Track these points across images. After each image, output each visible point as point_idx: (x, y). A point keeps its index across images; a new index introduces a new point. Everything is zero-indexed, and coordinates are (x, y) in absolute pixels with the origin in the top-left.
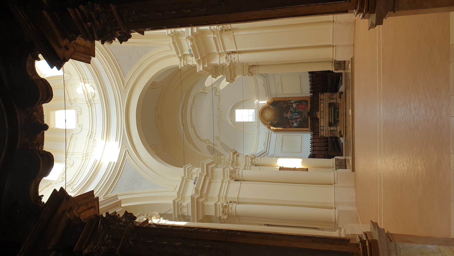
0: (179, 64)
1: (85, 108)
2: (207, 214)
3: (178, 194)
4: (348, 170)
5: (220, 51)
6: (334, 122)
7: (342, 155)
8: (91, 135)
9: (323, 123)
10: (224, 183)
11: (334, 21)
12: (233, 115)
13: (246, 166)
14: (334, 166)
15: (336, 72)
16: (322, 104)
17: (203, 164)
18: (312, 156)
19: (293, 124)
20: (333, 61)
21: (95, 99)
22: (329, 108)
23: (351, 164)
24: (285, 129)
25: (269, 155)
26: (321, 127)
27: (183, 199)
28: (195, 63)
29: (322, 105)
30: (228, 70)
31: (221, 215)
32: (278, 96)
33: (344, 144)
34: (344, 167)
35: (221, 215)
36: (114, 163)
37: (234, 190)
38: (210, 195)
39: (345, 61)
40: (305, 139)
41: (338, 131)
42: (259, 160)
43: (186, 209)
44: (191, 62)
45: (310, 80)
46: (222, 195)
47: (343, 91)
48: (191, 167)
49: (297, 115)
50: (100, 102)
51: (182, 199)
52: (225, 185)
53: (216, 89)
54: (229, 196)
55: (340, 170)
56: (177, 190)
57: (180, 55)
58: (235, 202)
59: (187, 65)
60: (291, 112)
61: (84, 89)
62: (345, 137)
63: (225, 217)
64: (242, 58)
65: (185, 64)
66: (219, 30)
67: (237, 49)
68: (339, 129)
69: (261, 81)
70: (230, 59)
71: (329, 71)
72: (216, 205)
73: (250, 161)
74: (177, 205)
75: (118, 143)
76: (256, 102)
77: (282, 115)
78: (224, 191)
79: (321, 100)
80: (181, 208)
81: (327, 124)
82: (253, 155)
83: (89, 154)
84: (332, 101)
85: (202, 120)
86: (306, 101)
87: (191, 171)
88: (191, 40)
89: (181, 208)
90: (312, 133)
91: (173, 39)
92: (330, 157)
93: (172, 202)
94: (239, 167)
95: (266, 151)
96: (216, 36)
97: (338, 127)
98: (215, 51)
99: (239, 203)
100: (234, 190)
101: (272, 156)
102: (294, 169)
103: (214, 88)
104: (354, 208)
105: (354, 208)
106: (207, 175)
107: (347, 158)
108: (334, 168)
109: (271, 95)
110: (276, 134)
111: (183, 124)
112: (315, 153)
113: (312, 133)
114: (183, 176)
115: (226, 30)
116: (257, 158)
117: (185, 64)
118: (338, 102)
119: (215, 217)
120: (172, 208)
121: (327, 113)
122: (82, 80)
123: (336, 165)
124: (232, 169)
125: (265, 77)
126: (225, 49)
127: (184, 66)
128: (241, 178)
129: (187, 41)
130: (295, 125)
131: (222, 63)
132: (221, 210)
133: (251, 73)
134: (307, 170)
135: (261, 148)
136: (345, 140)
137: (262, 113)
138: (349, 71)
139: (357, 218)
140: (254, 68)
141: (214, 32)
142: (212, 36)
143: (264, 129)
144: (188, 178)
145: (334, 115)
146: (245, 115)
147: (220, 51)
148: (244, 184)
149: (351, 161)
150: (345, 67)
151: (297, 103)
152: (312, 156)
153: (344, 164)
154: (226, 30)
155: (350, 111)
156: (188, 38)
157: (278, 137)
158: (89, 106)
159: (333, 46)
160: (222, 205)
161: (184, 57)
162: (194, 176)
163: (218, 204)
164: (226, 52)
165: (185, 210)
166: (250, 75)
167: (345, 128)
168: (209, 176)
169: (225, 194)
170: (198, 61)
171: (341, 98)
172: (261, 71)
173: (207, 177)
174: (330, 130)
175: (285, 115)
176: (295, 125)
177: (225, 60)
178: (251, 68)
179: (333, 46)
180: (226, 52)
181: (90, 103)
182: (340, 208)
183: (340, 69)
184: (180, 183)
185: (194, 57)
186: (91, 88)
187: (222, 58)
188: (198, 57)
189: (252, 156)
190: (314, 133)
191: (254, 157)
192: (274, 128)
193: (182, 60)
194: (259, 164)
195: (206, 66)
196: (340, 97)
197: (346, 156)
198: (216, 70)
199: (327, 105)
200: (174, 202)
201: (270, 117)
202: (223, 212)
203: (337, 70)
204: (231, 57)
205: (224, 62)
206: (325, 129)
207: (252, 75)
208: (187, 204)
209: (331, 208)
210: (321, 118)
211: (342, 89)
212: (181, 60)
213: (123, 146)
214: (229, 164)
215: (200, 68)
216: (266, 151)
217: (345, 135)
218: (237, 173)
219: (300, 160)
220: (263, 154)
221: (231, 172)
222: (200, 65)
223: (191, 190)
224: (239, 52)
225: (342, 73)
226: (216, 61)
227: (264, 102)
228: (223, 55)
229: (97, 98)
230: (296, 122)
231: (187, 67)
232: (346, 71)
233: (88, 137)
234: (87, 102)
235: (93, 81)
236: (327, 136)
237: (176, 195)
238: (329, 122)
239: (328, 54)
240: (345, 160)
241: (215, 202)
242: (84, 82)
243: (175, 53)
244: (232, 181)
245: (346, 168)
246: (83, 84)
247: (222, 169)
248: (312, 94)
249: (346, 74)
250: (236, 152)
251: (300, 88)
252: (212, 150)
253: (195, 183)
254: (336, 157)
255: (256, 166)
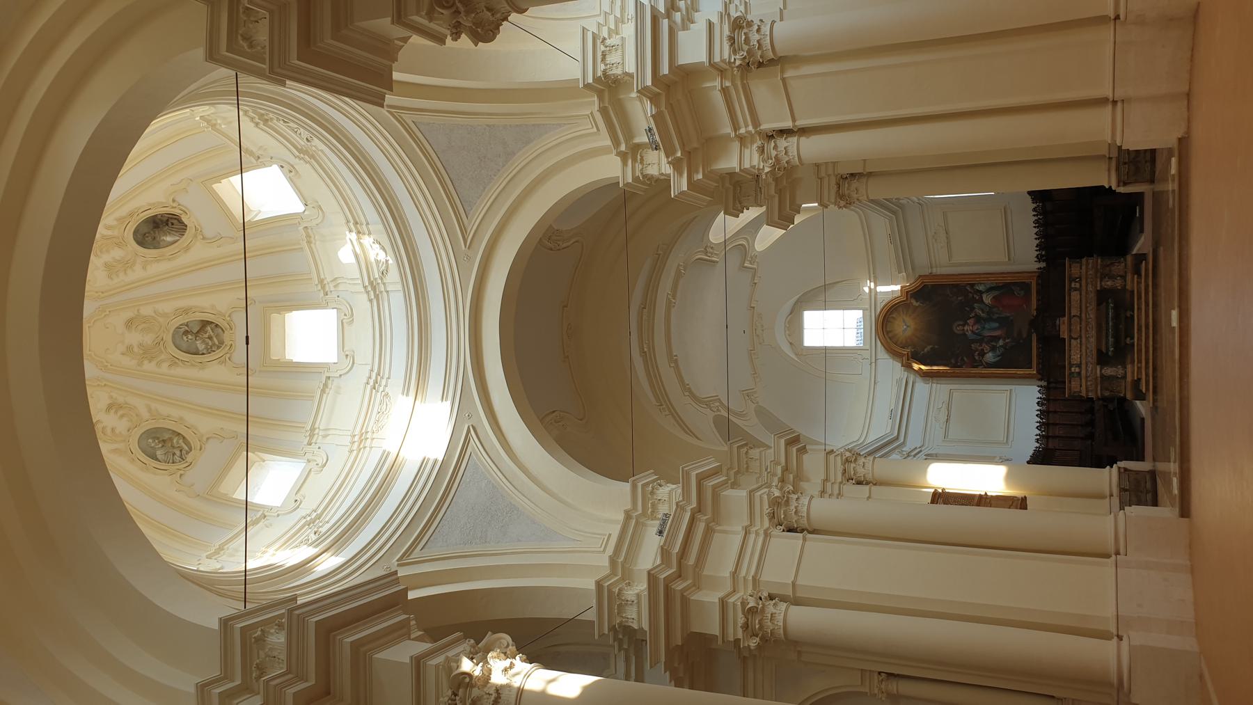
0: (619, 174)
1: (362, 304)
2: (696, 628)
3: (613, 561)
4: (1166, 512)
5: (743, 131)
6: (1116, 349)
7: (1141, 458)
8: (376, 382)
9: (1081, 353)
10: (753, 536)
11: (1117, 17)
12: (795, 327)
13: (829, 484)
14: (1115, 491)
15: (1122, 190)
16: (1073, 293)
17: (687, 475)
18: (1041, 457)
19: (983, 354)
20: (1114, 154)
21: (388, 279)
22: (1099, 304)
23: (1176, 491)
24: (957, 370)
25: (906, 449)
26: (1071, 365)
27: (628, 577)
28: (667, 169)
29: (1075, 296)
30: (772, 192)
31: (740, 635)
32: (934, 271)
33: (1148, 423)
34: (1149, 496)
35: (740, 635)
36: (436, 461)
37: (784, 561)
38: (707, 571)
39: (1153, 151)
40: (1019, 405)
41: (1129, 379)
42: (868, 466)
43: (635, 609)
44: (656, 167)
45: (1036, 222)
46: (743, 573)
47: (1148, 250)
48: (653, 481)
49: (995, 329)
50: (399, 287)
51: (623, 579)
52: (756, 542)
53: (744, 251)
54: (766, 577)
55: (1134, 511)
56: (610, 550)
57: (623, 148)
58: (784, 599)
59: (644, 176)
60: (978, 320)
61: (358, 250)
62: (1155, 401)
63: (753, 643)
64: (812, 148)
65: (638, 173)
66: (738, 63)
67: (794, 120)
68: (1131, 372)
69: (881, 224)
70: (774, 153)
71: (1099, 190)
72: (723, 603)
73: (840, 468)
74: (607, 595)
75: (448, 404)
76: (867, 290)
77: (946, 329)
78: (752, 554)
79: (1072, 280)
80: (620, 606)
81: (1093, 358)
82: (849, 450)
83: (369, 435)
84: (1109, 284)
85: (701, 339)
86: (1025, 287)
87: (652, 493)
88: (654, 99)
89: (620, 606)
90: (1044, 383)
91: (601, 99)
92: (1099, 462)
93: (593, 587)
94: (804, 485)
95: (897, 438)
96: (728, 84)
97: (1129, 367)
98: (728, 129)
99: (797, 602)
100: (784, 561)
101: (913, 454)
102: (982, 501)
103: (740, 247)
104: (1188, 643)
105: (1188, 643)
106: (699, 509)
107: (1161, 466)
108: (1116, 500)
109: (913, 269)
110: (928, 386)
111: (643, 353)
112: (1051, 446)
113: (1044, 383)
114: (629, 507)
115: (760, 65)
116: (861, 460)
117: (638, 173)
118: (1129, 287)
119: (720, 642)
120: (594, 602)
121: (1093, 323)
122: (351, 225)
123: (1122, 490)
124: (777, 493)
125: (894, 212)
126: (756, 123)
127: (635, 179)
128: (804, 523)
129: (641, 101)
130: (990, 357)
131: (747, 165)
132: (741, 620)
133: (844, 199)
134: (1022, 503)
135: (881, 428)
136: (1155, 408)
137: (884, 323)
138: (1171, 186)
139: (1201, 677)
140: (855, 184)
141: (722, 72)
142: (717, 83)
143: (891, 369)
144: (644, 513)
145: (1116, 327)
146: (834, 328)
147: (743, 131)
148: (816, 544)
149: (1175, 481)
150: (1153, 172)
151: (996, 293)
152: (1041, 457)
153: (1149, 485)
154: (760, 65)
155: (1175, 314)
156: (643, 92)
157: (932, 396)
158: (371, 301)
159: (1115, 102)
160: (744, 604)
161: (633, 153)
162: (663, 509)
163: (732, 600)
164: (759, 133)
165: (631, 613)
166: (842, 203)
167: (1155, 369)
168: (706, 509)
169: (752, 572)
170: (676, 164)
171: (1139, 275)
172: (878, 190)
173: (699, 516)
174: (1102, 376)
175: (957, 329)
176: (990, 357)
177: (756, 156)
178: (845, 183)
179: (1115, 102)
180: (759, 133)
181: (374, 290)
182: (1137, 637)
183: (1136, 182)
184: (619, 527)
185: (663, 154)
186: (376, 251)
187: (747, 152)
188: (674, 152)
189: (848, 454)
190: (1049, 383)
191: (852, 456)
192: (923, 367)
193: (630, 162)
194: (869, 477)
195: (700, 176)
196: (1137, 272)
197: (1154, 460)
198: (736, 191)
199: (1092, 296)
200: (599, 584)
201: (909, 332)
202: (746, 627)
203: (1125, 184)
204: (776, 147)
205: (755, 162)
206: (1084, 373)
207: (849, 204)
208: (638, 595)
209: (1104, 635)
210: (1071, 338)
211: (1142, 244)
212: (625, 163)
213: (461, 413)
214: (774, 475)
215: (680, 184)
216: (897, 438)
217: (1155, 392)
218: (793, 507)
219: (1000, 471)
220: (883, 448)
221: (775, 503)
222: (680, 174)
223: (648, 555)
224: (804, 131)
225: (1141, 195)
226: (731, 162)
227: (891, 289)
228: (752, 142)
229: (393, 276)
230: (993, 349)
231: (643, 183)
232: (1159, 187)
233: (369, 387)
234: (365, 287)
235: (381, 227)
236: (1091, 395)
237: (606, 563)
238: (1099, 352)
239: (1097, 128)
240: (1153, 474)
241: (721, 594)
242: (359, 232)
243: (608, 142)
244: (777, 532)
245: (1155, 503)
246: (353, 236)
247: (744, 493)
248: (1043, 265)
249: (1158, 197)
250: (794, 441)
251: (997, 243)
252: (727, 429)
253: (660, 533)
254: (1122, 464)
255: (859, 483)
